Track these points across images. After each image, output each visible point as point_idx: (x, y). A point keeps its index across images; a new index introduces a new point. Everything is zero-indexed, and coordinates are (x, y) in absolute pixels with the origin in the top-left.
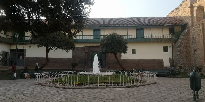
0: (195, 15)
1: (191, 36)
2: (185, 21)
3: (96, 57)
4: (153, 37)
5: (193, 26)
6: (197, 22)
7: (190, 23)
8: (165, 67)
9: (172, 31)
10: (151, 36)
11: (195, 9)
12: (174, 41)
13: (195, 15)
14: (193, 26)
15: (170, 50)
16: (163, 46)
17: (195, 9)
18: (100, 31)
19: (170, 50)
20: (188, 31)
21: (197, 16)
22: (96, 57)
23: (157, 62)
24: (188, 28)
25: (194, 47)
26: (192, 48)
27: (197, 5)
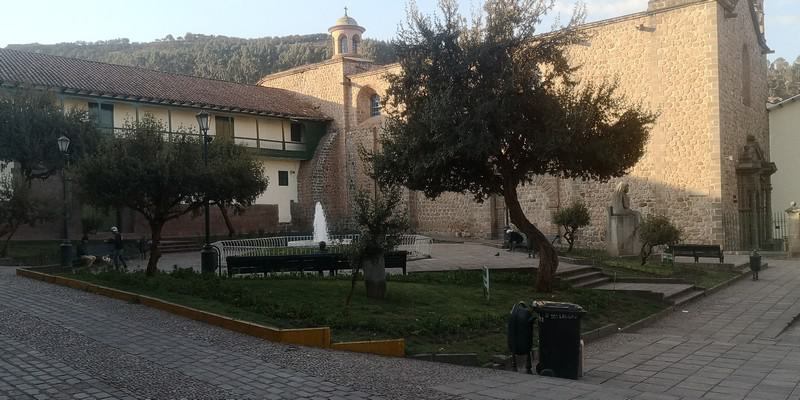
0: (354, 104)
1: (344, 152)
2: (328, 113)
3: (319, 207)
4: (263, 145)
5: (348, 128)
6: (359, 122)
7: (341, 121)
8: (281, 224)
9: (297, 130)
10: (258, 144)
11: (355, 91)
12: (304, 158)
13: (354, 104)
14: (348, 128)
15: (292, 179)
16: (593, 222)
17: (355, 91)
18: (112, 110)
19: (292, 179)
20: (337, 139)
21: (358, 107)
22: (319, 207)
23: (264, 212)
24: (335, 131)
25: (349, 177)
26: (345, 180)
27: (362, 84)
